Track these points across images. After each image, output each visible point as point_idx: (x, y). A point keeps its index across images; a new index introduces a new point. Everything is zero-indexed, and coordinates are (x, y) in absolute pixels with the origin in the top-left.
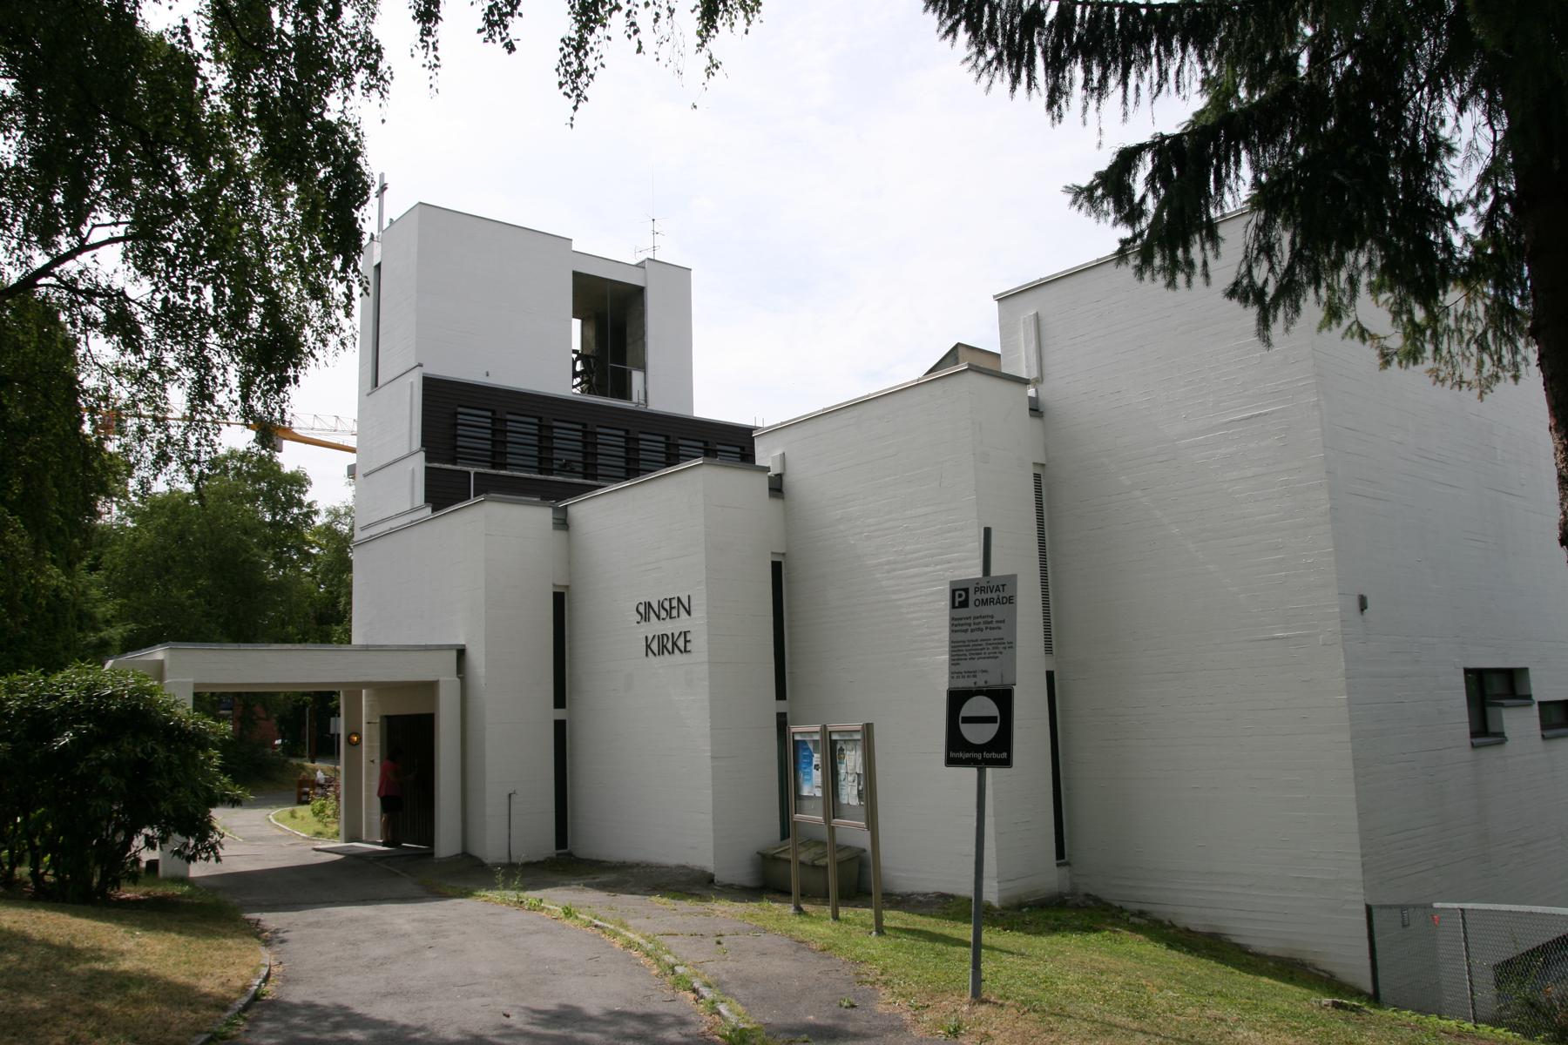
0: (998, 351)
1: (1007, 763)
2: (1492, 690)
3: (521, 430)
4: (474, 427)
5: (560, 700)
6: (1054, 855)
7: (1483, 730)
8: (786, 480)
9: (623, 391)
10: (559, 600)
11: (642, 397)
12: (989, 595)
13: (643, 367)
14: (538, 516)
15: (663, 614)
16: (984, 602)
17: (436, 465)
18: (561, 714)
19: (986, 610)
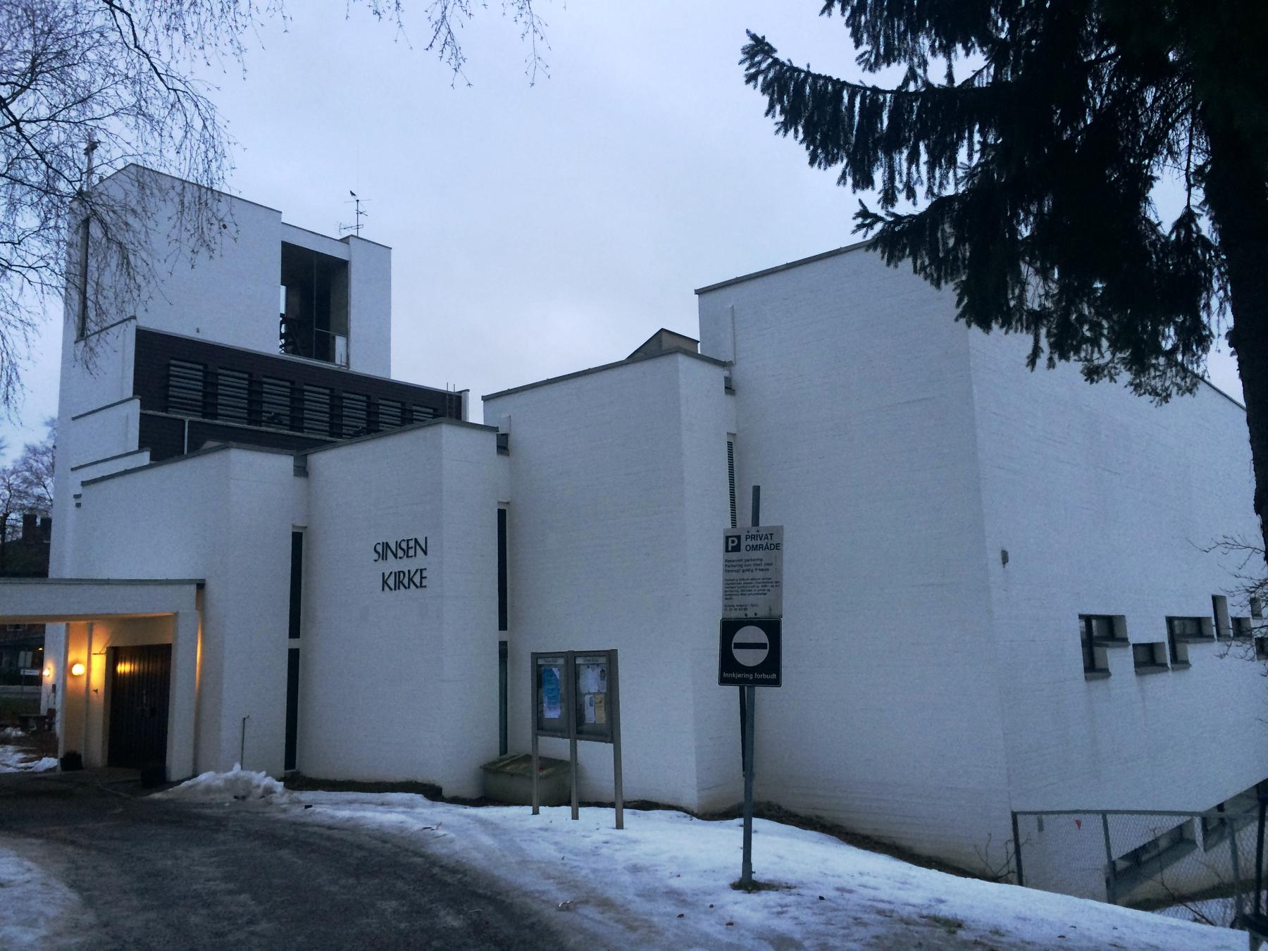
1: (777, 682)
3: (232, 385)
4: (186, 381)
5: (294, 631)
9: (326, 352)
10: (297, 539)
11: (344, 359)
12: (759, 542)
13: (345, 333)
14: (283, 463)
15: (400, 553)
16: (755, 548)
17: (150, 412)
18: (295, 643)
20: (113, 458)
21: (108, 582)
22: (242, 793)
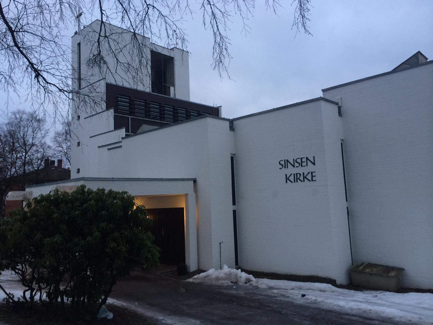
6: (234, 263)
13: (174, 85)
20: (108, 132)
21: (138, 179)
22: (234, 280)
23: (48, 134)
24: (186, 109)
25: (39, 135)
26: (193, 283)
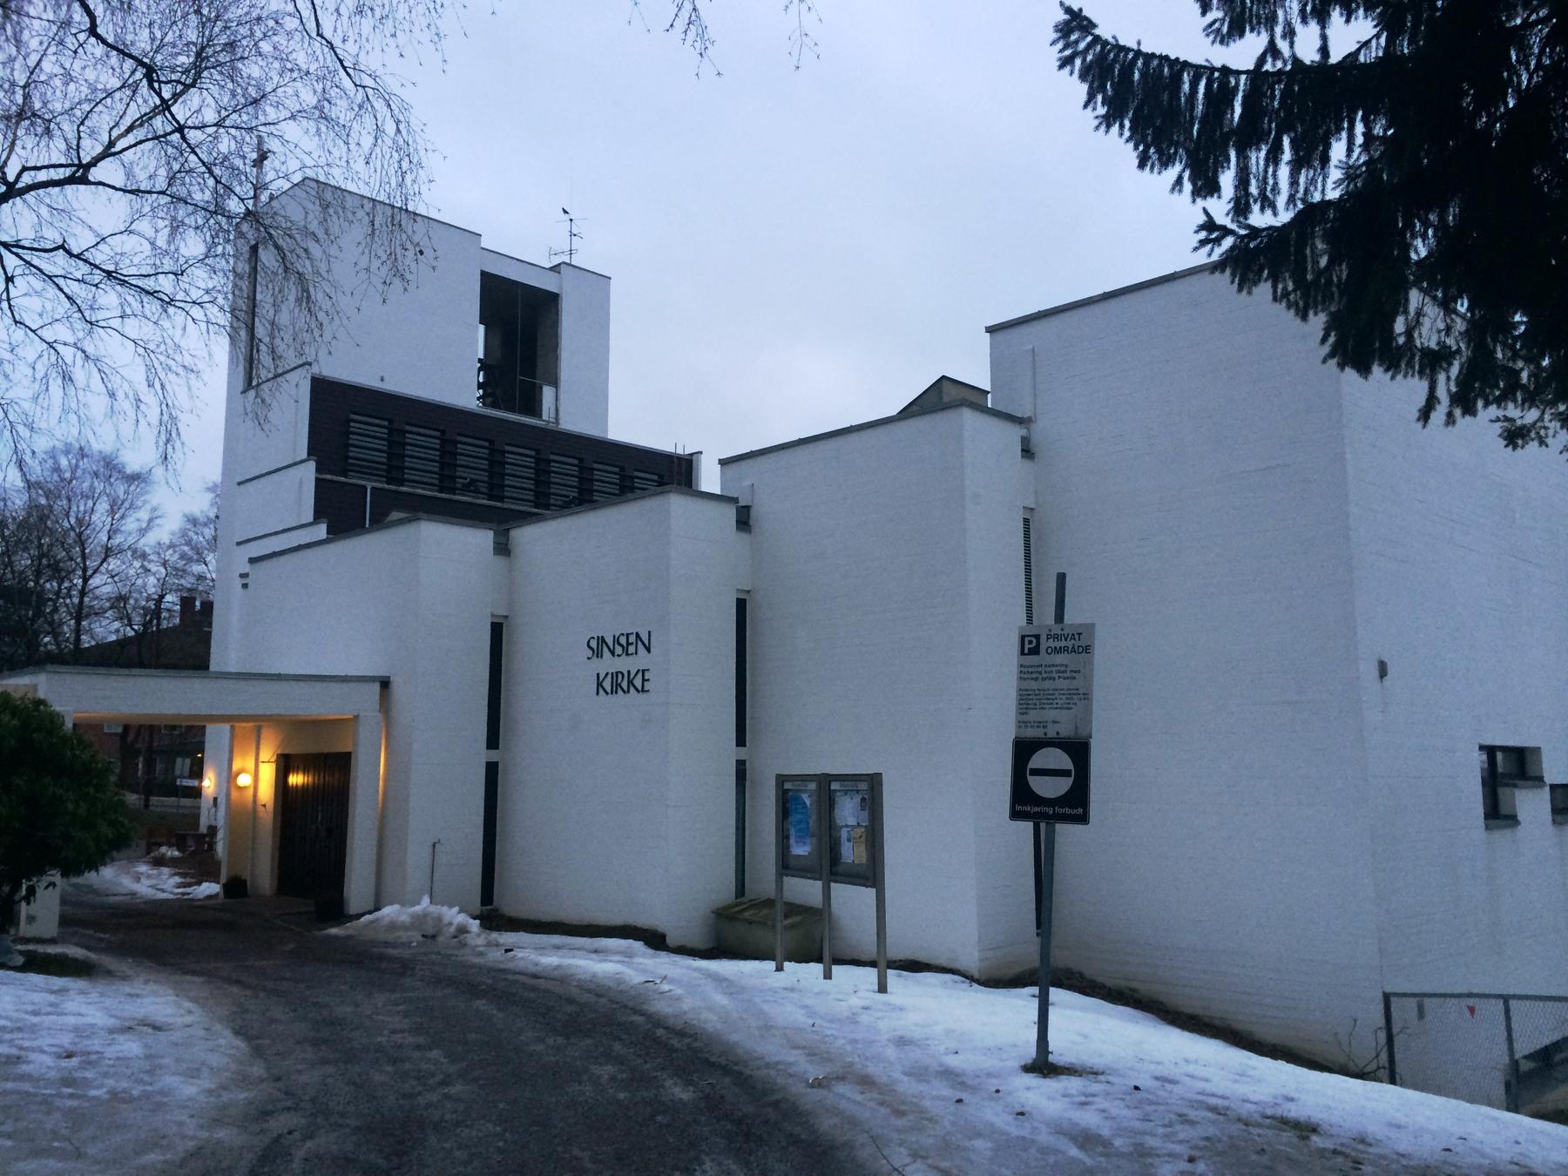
0: (986, 385)
1: (1083, 819)
2: (1508, 769)
3: (422, 445)
4: (368, 439)
5: (493, 741)
7: (1497, 814)
8: (753, 513)
9: (533, 407)
10: (497, 630)
11: (553, 414)
12: (1063, 644)
13: (554, 382)
14: (483, 538)
15: (619, 650)
16: (1058, 651)
17: (329, 477)
18: (494, 756)
19: (1059, 659)
22: (431, 931)
23: (158, 521)
24: (581, 460)
25: (130, 525)
26: (336, 937)
